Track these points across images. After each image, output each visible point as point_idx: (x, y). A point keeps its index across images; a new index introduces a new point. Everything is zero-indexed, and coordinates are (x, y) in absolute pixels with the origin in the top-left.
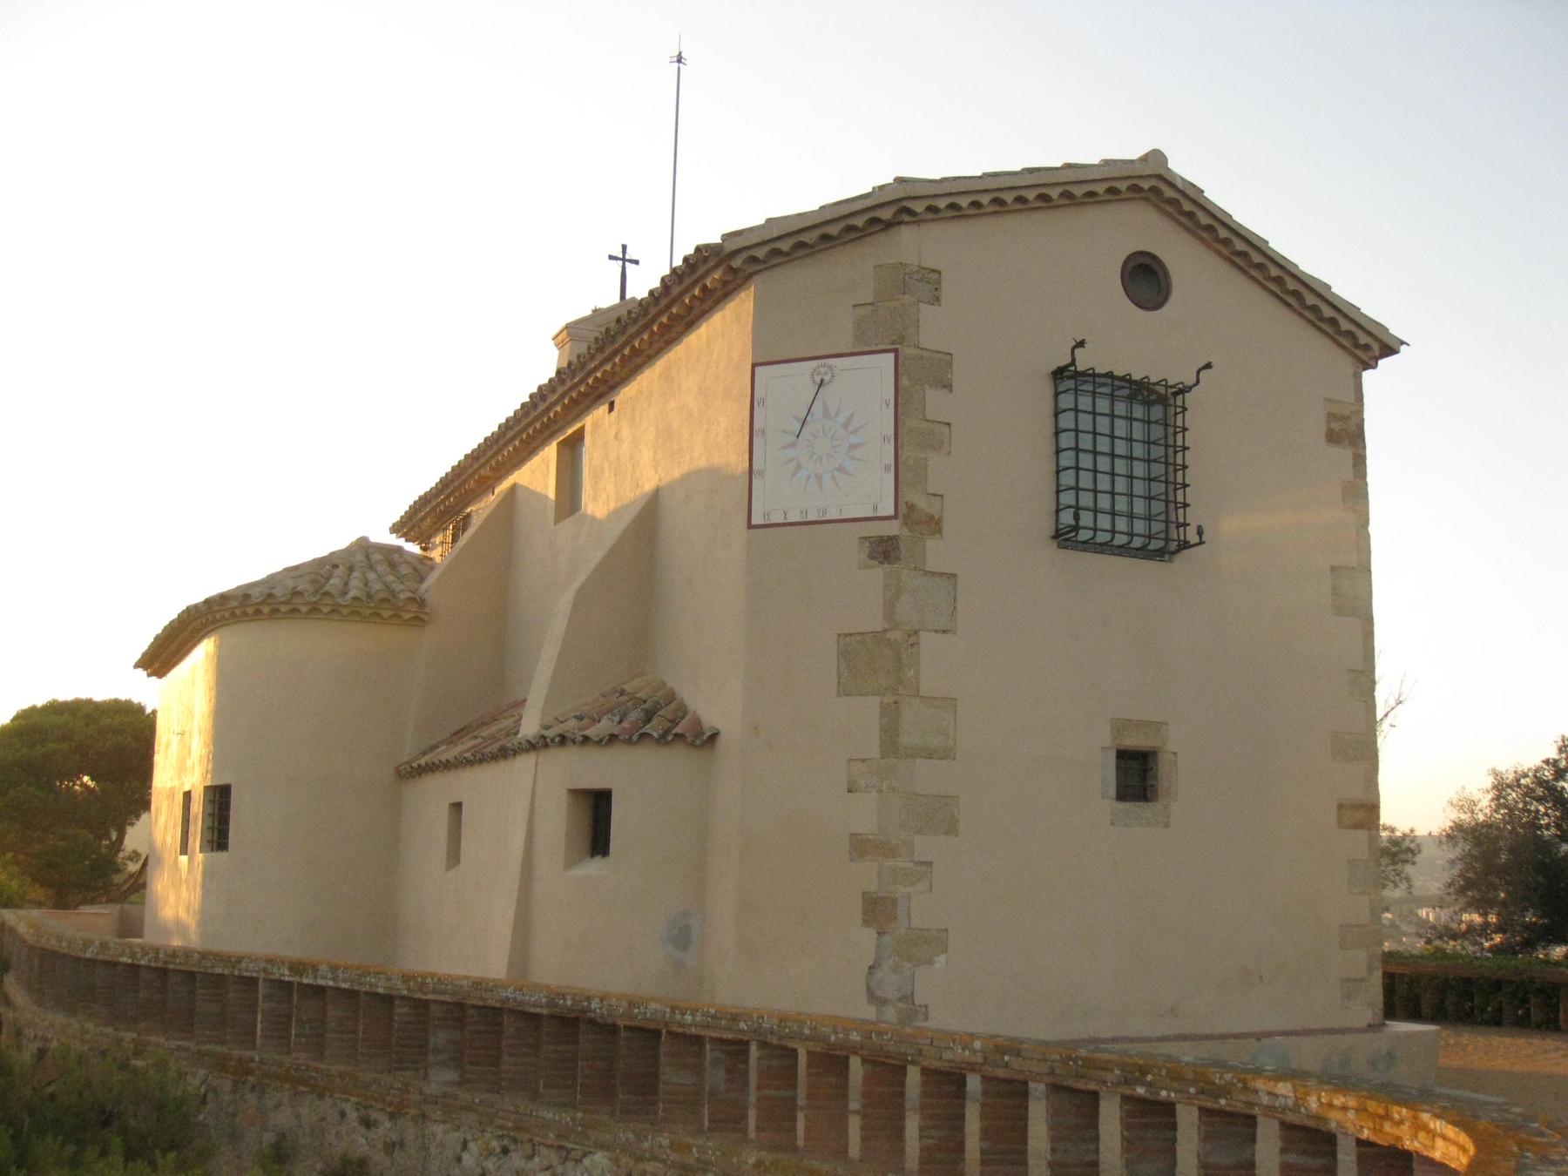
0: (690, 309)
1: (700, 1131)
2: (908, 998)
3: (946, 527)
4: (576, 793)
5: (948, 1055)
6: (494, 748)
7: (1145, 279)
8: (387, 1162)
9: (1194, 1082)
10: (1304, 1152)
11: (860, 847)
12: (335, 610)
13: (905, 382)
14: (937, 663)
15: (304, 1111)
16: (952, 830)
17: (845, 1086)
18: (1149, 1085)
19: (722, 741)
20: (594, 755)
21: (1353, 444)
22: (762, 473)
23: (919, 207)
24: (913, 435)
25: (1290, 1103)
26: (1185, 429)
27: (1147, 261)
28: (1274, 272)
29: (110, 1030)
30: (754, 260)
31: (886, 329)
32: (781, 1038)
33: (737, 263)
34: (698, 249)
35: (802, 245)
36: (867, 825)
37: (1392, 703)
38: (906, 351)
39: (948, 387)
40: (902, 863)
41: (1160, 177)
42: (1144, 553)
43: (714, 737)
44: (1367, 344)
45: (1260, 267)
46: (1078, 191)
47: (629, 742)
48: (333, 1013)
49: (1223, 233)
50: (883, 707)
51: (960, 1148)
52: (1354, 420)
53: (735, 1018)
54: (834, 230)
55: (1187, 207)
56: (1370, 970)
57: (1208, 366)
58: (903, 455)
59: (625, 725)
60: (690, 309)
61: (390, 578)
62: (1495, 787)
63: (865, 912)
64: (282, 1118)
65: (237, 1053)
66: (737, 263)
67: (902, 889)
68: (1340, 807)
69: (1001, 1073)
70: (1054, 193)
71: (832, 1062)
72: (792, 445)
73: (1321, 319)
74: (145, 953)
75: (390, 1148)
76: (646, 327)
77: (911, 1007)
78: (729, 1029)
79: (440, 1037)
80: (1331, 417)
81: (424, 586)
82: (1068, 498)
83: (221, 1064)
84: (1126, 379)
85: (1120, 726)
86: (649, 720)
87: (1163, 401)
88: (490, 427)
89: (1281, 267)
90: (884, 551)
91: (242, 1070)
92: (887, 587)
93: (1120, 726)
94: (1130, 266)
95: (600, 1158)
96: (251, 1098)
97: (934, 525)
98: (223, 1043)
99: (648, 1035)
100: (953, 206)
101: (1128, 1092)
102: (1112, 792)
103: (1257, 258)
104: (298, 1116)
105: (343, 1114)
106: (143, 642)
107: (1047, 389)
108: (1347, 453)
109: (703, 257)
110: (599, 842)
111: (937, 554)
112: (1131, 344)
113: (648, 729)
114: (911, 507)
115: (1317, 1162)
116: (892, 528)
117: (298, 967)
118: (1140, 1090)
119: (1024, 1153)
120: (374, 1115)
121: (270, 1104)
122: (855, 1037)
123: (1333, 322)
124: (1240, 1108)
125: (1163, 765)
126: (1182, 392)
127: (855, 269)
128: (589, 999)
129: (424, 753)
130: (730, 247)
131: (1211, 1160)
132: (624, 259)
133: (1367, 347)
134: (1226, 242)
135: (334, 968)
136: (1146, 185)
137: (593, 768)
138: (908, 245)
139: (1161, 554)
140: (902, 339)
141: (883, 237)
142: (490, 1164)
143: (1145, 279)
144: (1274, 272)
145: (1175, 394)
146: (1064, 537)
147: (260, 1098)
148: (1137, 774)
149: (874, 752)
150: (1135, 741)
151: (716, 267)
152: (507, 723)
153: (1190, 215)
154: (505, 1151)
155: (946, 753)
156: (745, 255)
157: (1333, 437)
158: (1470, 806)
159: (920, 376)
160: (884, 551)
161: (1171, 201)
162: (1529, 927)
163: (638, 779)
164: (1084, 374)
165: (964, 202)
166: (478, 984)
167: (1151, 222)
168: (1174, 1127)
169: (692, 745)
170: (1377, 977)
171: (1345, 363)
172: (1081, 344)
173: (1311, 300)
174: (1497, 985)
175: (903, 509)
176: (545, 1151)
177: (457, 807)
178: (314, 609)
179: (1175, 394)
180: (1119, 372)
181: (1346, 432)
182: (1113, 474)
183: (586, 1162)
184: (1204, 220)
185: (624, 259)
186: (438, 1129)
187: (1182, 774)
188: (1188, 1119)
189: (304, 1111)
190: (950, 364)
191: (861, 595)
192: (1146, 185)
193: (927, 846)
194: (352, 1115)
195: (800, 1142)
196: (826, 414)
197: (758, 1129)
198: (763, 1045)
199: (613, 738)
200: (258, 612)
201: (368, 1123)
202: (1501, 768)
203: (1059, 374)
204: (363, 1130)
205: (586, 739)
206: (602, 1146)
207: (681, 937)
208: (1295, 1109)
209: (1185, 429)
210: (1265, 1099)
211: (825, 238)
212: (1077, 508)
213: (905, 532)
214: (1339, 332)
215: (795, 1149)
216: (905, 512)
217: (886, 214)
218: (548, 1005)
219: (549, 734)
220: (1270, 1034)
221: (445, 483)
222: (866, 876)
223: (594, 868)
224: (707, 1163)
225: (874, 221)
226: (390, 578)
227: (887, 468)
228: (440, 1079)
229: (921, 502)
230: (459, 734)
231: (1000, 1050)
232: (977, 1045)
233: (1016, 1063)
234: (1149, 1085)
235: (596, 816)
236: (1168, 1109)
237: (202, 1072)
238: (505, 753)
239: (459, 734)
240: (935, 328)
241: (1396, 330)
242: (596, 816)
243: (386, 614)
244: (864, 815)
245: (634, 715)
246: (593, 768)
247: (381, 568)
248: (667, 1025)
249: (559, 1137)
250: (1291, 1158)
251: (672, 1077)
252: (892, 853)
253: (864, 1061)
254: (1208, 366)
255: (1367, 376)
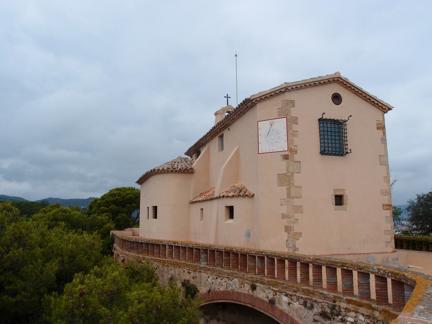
0: (244, 110)
1: (256, 274)
2: (294, 246)
3: (298, 152)
4: (227, 207)
5: (305, 260)
6: (209, 198)
7: (337, 99)
8: (193, 280)
9: (356, 266)
10: (380, 281)
11: (284, 216)
12: (176, 171)
13: (288, 123)
14: (297, 179)
15: (176, 270)
16: (302, 212)
17: (285, 266)
18: (347, 267)
19: (255, 196)
20: (229, 199)
21: (383, 129)
22: (261, 143)
23: (290, 88)
24: (291, 134)
25: (377, 271)
26: (346, 129)
27: (337, 95)
28: (364, 95)
29: (137, 255)
30: (257, 101)
31: (284, 113)
32: (272, 256)
33: (253, 101)
34: (246, 99)
35: (266, 97)
36: (285, 211)
37: (394, 181)
38: (288, 117)
39: (297, 124)
40: (292, 220)
41: (339, 77)
42: (338, 155)
43: (253, 195)
44: (384, 108)
45: (361, 94)
46: (322, 82)
47: (237, 197)
48: (181, 251)
49: (353, 88)
50: (287, 188)
51: (308, 278)
52: (383, 125)
53: (262, 252)
54: (273, 94)
55: (345, 83)
56: (392, 240)
57: (351, 116)
58: (289, 138)
59: (236, 193)
60: (244, 110)
61: (186, 164)
62: (418, 198)
63: (285, 229)
64: (172, 272)
65: (163, 259)
66: (253, 101)
67: (292, 225)
68: (383, 205)
69: (316, 264)
70: (317, 83)
71: (282, 261)
72: (266, 137)
73: (375, 104)
74: (144, 240)
75: (193, 278)
76: (235, 114)
77: (296, 249)
78: (261, 255)
79: (203, 256)
80: (378, 124)
81: (193, 166)
82: (323, 145)
83: (160, 261)
84: (334, 120)
85: (335, 190)
86: (240, 192)
87: (341, 123)
88: (204, 134)
89: (366, 94)
90: (286, 157)
91: (164, 262)
92: (287, 165)
93: (335, 190)
94: (334, 96)
95: (236, 279)
96: (166, 268)
97: (296, 152)
98: (160, 257)
99: (244, 255)
100: (296, 87)
101: (343, 268)
102: (334, 204)
103: (360, 92)
104: (175, 272)
105: (184, 271)
106: (137, 179)
107: (317, 123)
108: (381, 132)
109: (247, 101)
110: (231, 216)
111: (297, 157)
112: (334, 112)
113: (240, 194)
114: (291, 148)
115: (383, 283)
116: (287, 153)
117: (174, 243)
118: (345, 268)
119: (322, 280)
120: (191, 271)
121: (169, 269)
122: (286, 256)
123: (377, 104)
124: (366, 272)
125: (345, 198)
126: (345, 121)
127: (278, 102)
128: (232, 248)
129: (195, 199)
130: (252, 98)
131: (361, 282)
132: (227, 97)
133: (385, 109)
134: (354, 89)
135: (181, 243)
136: (336, 79)
137: (230, 202)
138: (288, 96)
139: (342, 155)
140: (287, 115)
141: (282, 95)
142: (214, 281)
143: (337, 99)
144: (364, 95)
145: (344, 122)
146: (323, 153)
147: (168, 268)
148: (339, 200)
149: (286, 197)
150: (339, 193)
151: (249, 102)
152: (211, 192)
153: (346, 85)
154: (217, 278)
155: (300, 197)
156: (255, 100)
157: (378, 128)
158: (413, 203)
159: (291, 122)
160: (286, 157)
161: (341, 82)
162: (428, 228)
163: (239, 205)
164: (325, 119)
165: (299, 86)
166: (210, 246)
167: (339, 87)
168: (352, 275)
169: (249, 197)
170: (393, 241)
171: (381, 112)
172: (324, 114)
173: (372, 100)
174: (421, 242)
175: (289, 149)
176: (225, 278)
177: (202, 209)
178: (172, 171)
179: (344, 122)
180: (332, 118)
181: (381, 127)
182: (331, 136)
183: (233, 280)
184: (349, 85)
185: (227, 97)
186: (203, 274)
187: (349, 199)
188: (355, 274)
189: (176, 270)
190: (297, 119)
191: (282, 167)
192: (336, 79)
193: (297, 216)
194: (186, 271)
195: (276, 276)
196: (273, 131)
197: (267, 274)
198: (268, 257)
199: (233, 196)
200: (161, 172)
201: (189, 273)
202: (419, 194)
203: (320, 120)
204: (188, 274)
205: (228, 196)
206: (236, 277)
207: (248, 235)
208: (378, 273)
209: (346, 129)
210: (371, 270)
211: (271, 95)
212: (325, 147)
213: (290, 153)
214: (379, 106)
215: (275, 278)
216: (290, 149)
217: (283, 90)
218: (224, 250)
219: (221, 195)
220: (370, 253)
221: (195, 145)
222: (285, 222)
223: (231, 221)
224: (258, 281)
225: (281, 92)
226: (186, 164)
227: (286, 141)
228: (203, 264)
229: (292, 147)
230: (201, 195)
231: (317, 259)
232: (311, 258)
233: (319, 262)
234: (347, 267)
235: (231, 210)
236: (351, 272)
237: (156, 263)
238: (212, 199)
239: (201, 195)
240: (294, 112)
241: (391, 104)
242: (231, 210)
243: (186, 172)
244: (284, 210)
245: (238, 191)
246: (230, 202)
247: (184, 162)
248: (248, 253)
249: (228, 275)
250: (377, 282)
251: (249, 263)
252: (290, 218)
253: (288, 261)
254: (351, 116)
255: (385, 115)
